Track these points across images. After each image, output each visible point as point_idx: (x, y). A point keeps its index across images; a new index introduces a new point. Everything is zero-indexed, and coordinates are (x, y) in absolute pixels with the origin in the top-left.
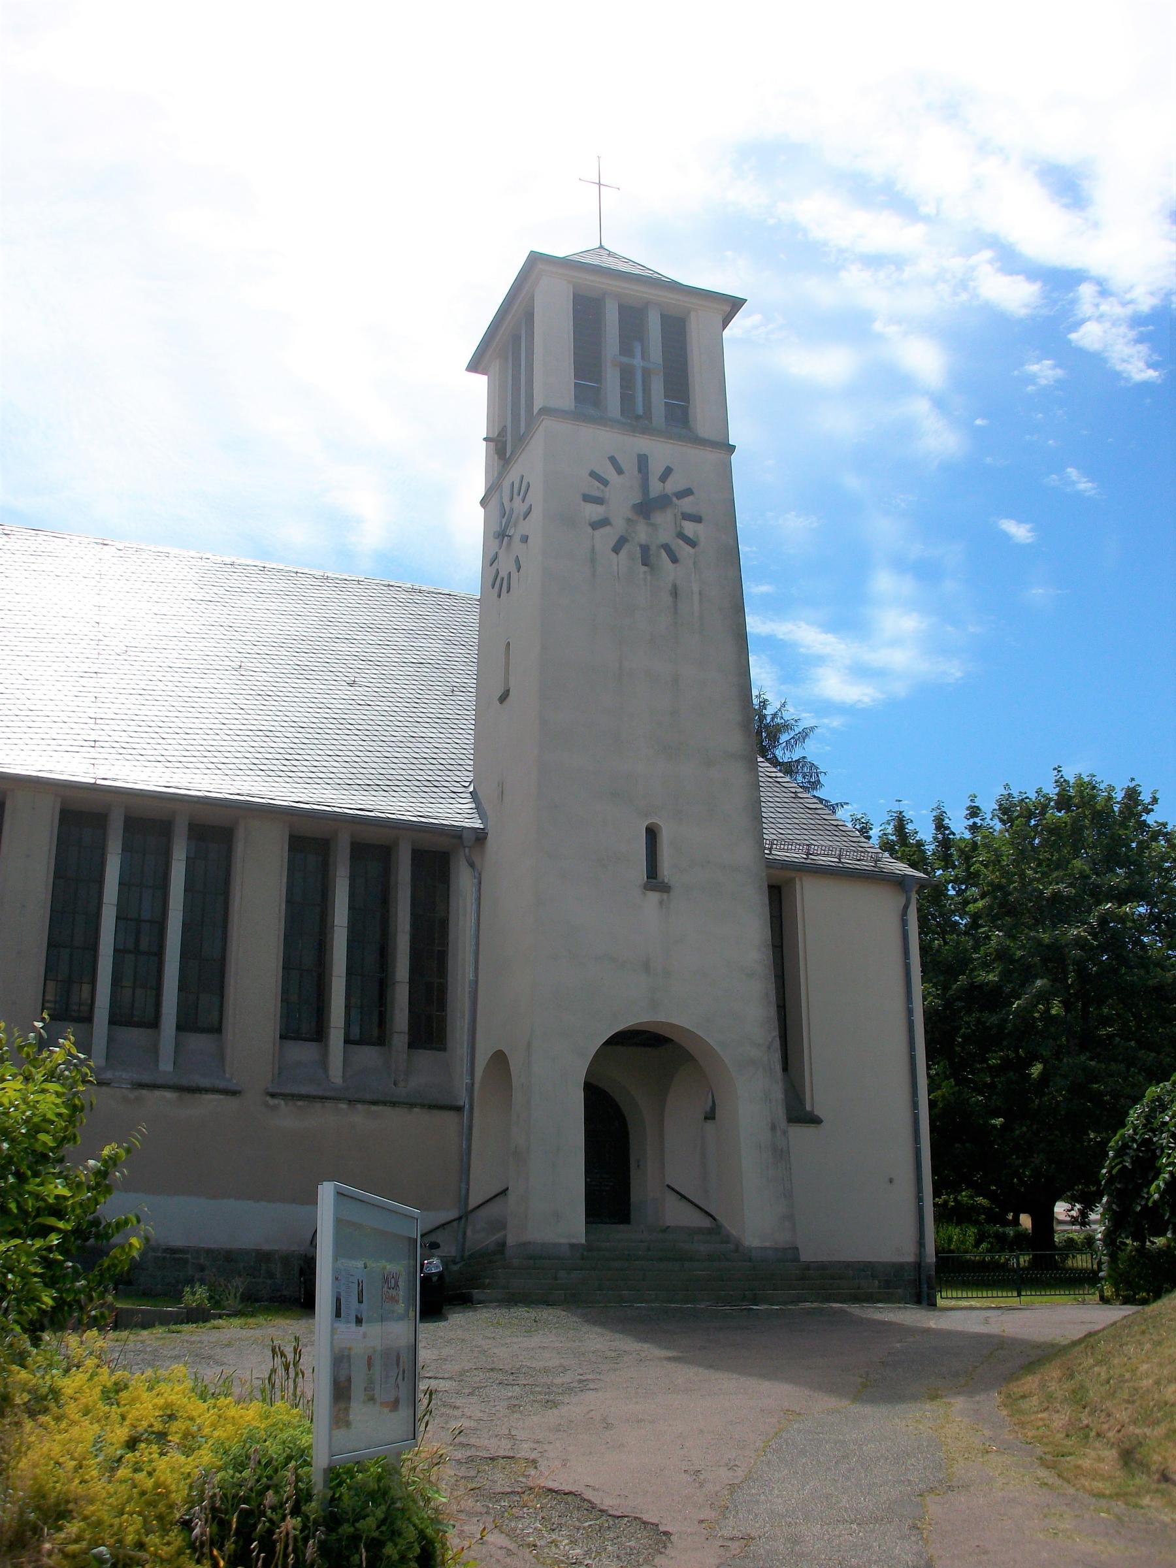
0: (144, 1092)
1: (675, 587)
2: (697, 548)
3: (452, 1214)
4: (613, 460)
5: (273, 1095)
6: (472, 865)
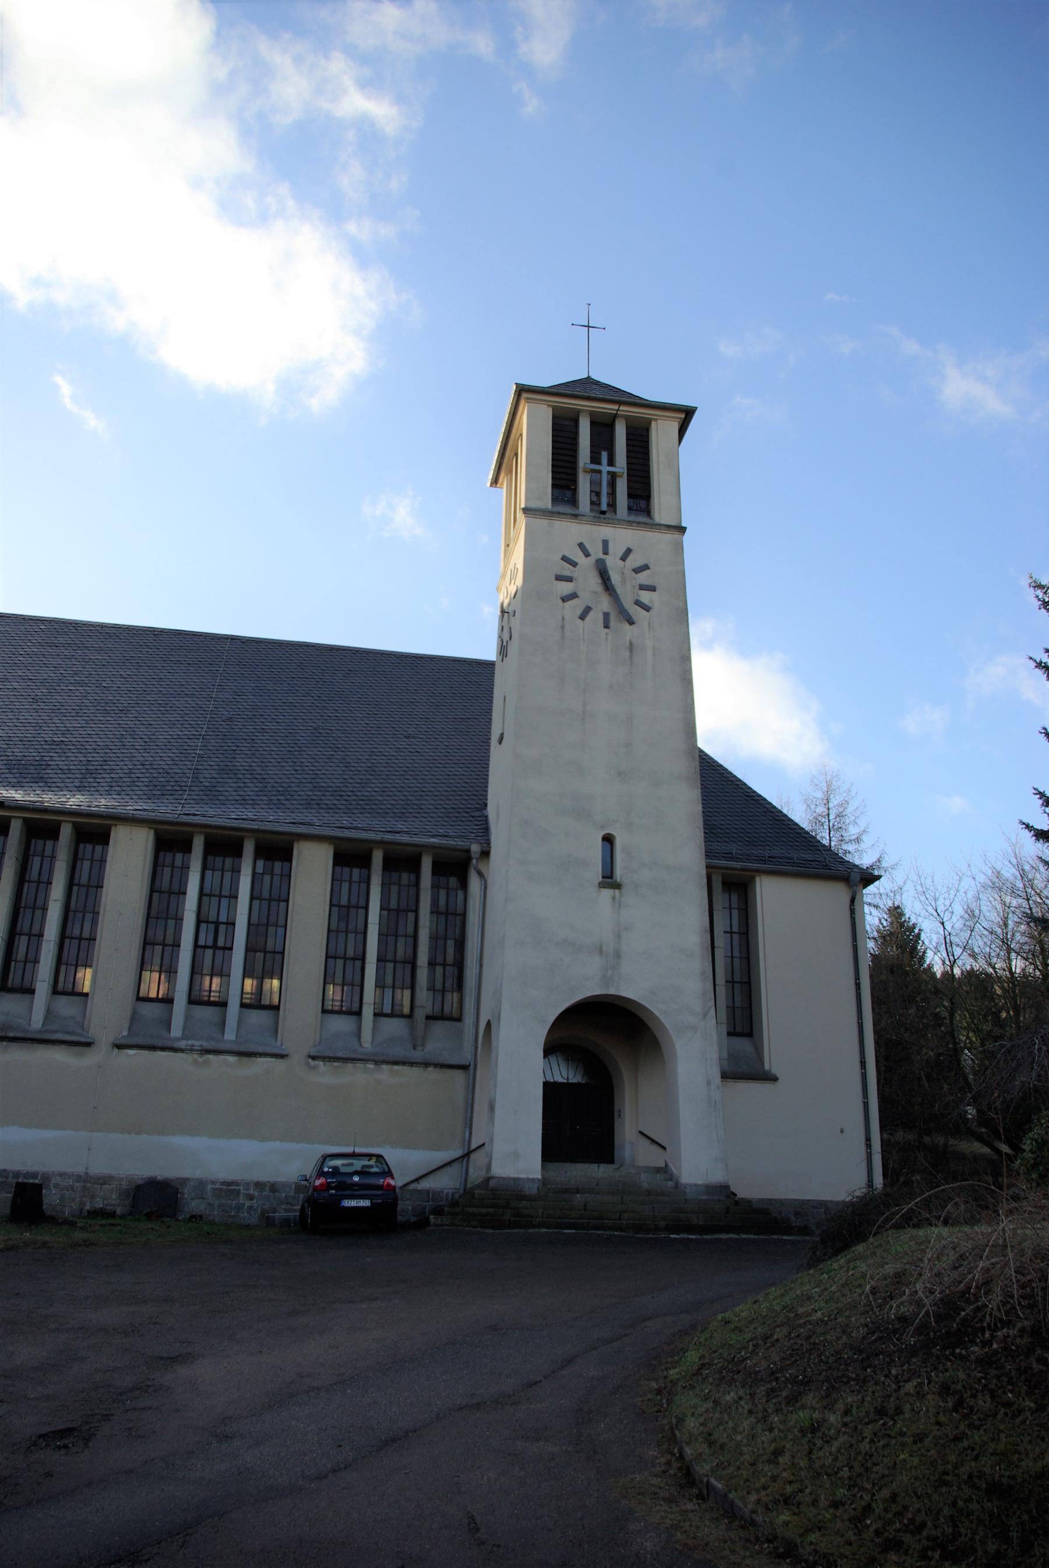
0: (211, 1057)
1: (631, 644)
2: (651, 611)
3: (458, 1153)
4: (581, 545)
5: (314, 1058)
6: (480, 874)
